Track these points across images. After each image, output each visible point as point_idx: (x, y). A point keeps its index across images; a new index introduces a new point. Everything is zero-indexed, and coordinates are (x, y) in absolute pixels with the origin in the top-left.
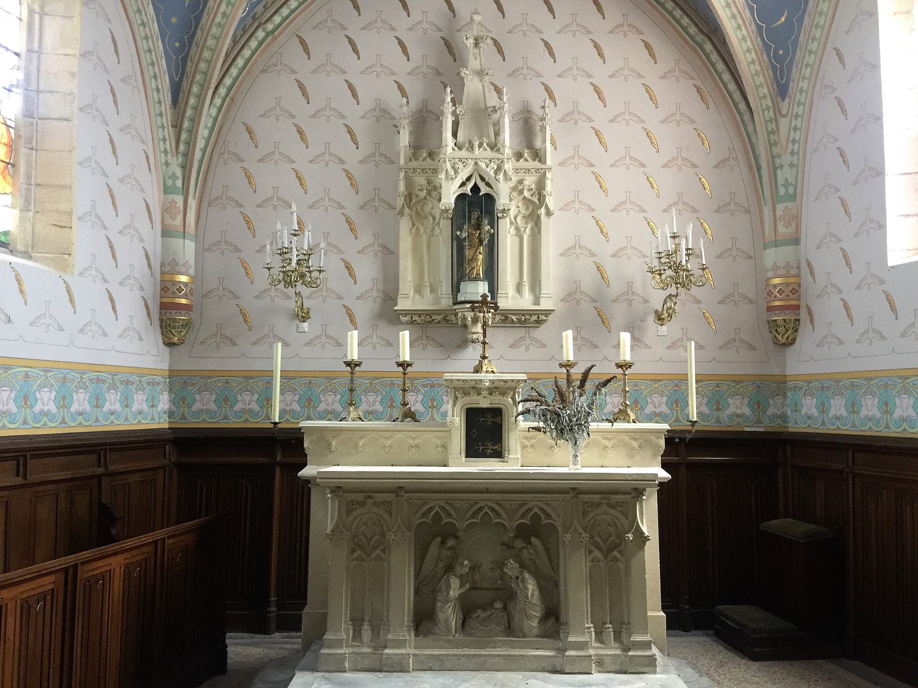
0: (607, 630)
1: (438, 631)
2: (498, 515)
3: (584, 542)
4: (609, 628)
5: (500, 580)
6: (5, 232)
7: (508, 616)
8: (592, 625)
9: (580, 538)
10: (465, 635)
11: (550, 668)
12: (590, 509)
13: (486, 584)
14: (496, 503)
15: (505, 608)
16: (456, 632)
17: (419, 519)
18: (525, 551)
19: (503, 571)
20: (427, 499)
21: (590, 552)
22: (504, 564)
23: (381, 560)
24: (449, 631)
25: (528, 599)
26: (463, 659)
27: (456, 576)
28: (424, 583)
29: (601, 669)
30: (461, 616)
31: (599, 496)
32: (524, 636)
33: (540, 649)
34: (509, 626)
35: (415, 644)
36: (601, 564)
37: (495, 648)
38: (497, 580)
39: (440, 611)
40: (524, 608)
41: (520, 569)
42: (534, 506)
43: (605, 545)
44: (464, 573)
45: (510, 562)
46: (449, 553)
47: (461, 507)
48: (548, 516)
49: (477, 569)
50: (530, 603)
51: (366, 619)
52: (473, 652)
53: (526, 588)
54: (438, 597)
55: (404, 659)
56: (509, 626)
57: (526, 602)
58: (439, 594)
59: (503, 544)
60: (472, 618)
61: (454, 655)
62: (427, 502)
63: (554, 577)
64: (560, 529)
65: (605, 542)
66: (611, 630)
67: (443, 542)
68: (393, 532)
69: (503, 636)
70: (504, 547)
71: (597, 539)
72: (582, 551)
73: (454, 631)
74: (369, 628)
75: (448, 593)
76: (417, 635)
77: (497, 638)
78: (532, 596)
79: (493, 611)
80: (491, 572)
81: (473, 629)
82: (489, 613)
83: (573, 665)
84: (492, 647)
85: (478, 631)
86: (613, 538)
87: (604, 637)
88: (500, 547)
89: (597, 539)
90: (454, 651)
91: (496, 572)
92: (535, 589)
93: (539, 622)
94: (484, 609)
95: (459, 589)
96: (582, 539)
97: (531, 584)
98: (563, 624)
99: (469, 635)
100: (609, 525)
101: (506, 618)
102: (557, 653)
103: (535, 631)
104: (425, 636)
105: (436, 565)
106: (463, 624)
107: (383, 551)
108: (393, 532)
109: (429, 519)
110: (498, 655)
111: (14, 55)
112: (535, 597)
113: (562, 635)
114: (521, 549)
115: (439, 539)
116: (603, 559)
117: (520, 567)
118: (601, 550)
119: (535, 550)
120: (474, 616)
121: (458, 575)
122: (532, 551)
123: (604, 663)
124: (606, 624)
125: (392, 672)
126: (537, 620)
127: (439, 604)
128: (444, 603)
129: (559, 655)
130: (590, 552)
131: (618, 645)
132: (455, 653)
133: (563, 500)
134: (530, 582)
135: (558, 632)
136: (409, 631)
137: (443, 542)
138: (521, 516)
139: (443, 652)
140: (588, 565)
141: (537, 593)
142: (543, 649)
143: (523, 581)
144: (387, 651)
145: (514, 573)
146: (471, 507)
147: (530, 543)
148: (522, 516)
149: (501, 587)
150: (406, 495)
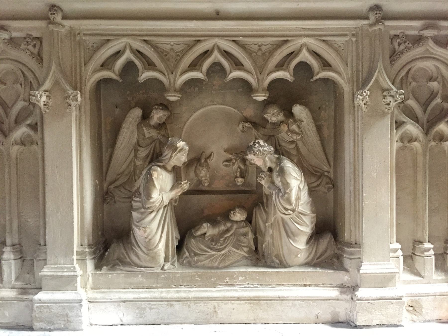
0: (426, 253)
1: (134, 258)
2: (238, 65)
3: (393, 104)
4: (428, 250)
5: (242, 177)
6: (306, 286)
7: (255, 232)
8: (398, 246)
9: (384, 97)
10: (182, 264)
11: (328, 317)
12: (402, 47)
13: (219, 185)
14: (234, 41)
15: (249, 220)
16: (166, 260)
17: (95, 71)
18: (284, 128)
19: (244, 161)
20: (109, 35)
21: (399, 124)
22: (250, 148)
23: (32, 143)
24: (154, 258)
25: (291, 204)
26: (177, 305)
27: (164, 168)
28: (118, 183)
29: (415, 318)
30: (176, 235)
31: (417, 24)
32: (283, 265)
33: (310, 285)
34: (256, 248)
35: (94, 283)
36: (416, 144)
37: (232, 285)
38: (236, 177)
39: (137, 226)
40: (283, 219)
41: (277, 156)
42: (302, 46)
43: (425, 111)
44: (180, 165)
45: (259, 143)
46: (153, 133)
47: (172, 49)
48: (324, 66)
49: (203, 161)
50: (294, 211)
51: (8, 242)
52: (194, 293)
53: (287, 185)
54: (134, 204)
55: (71, 308)
56: (256, 248)
57: (286, 209)
58: (135, 199)
59: (246, 120)
60: (195, 237)
61: (162, 300)
62: (108, 40)
63: (328, 172)
64: (346, 88)
65: (425, 105)
66: (432, 252)
67: (146, 117)
68: (46, 91)
69: (248, 265)
70: (247, 125)
71: (411, 103)
72: (387, 121)
73: (162, 260)
74: (12, 257)
75: (149, 196)
76: (98, 267)
77: (237, 270)
78: (298, 198)
79: (229, 225)
80: (226, 166)
81: (196, 254)
82: (223, 228)
83: (370, 313)
84: (227, 285)
85: (202, 258)
86: (438, 100)
87: (418, 265)
88: (241, 126)
89: (411, 103)
90: (162, 292)
91: (234, 164)
92: (302, 187)
93: (308, 242)
94: (214, 222)
95: (172, 189)
96: (389, 99)
97: (297, 179)
98: (350, 245)
99: (190, 265)
100: (431, 79)
101: (251, 236)
102: (341, 293)
103: (302, 257)
104: (113, 267)
105: (136, 156)
106: (180, 248)
107: (34, 127)
108: (46, 91)
109: (114, 72)
110: (239, 299)
111: (328, 328)
112: (301, 202)
113: (347, 263)
114: (276, 125)
115: (137, 113)
116: (421, 136)
117: (277, 151)
118: (416, 119)
119: (299, 127)
120: (199, 233)
121: (169, 168)
122: (294, 127)
123: (421, 307)
124: (421, 242)
125: (50, 330)
126: (304, 239)
127: (135, 214)
128: (142, 213)
129: (344, 297)
130: (399, 124)
131: (444, 277)
132: (164, 295)
133: (353, 35)
134: (294, 174)
135: (339, 257)
136: (82, 261)
137: (146, 117)
138: (277, 66)
139: (144, 294)
140: (396, 146)
141: (304, 195)
142: (317, 285)
143: (282, 172)
144: (42, 296)
145: (264, 161)
146: (190, 49)
147: (290, 114)
148: (280, 66)
149: (244, 188)
150: (67, 23)
